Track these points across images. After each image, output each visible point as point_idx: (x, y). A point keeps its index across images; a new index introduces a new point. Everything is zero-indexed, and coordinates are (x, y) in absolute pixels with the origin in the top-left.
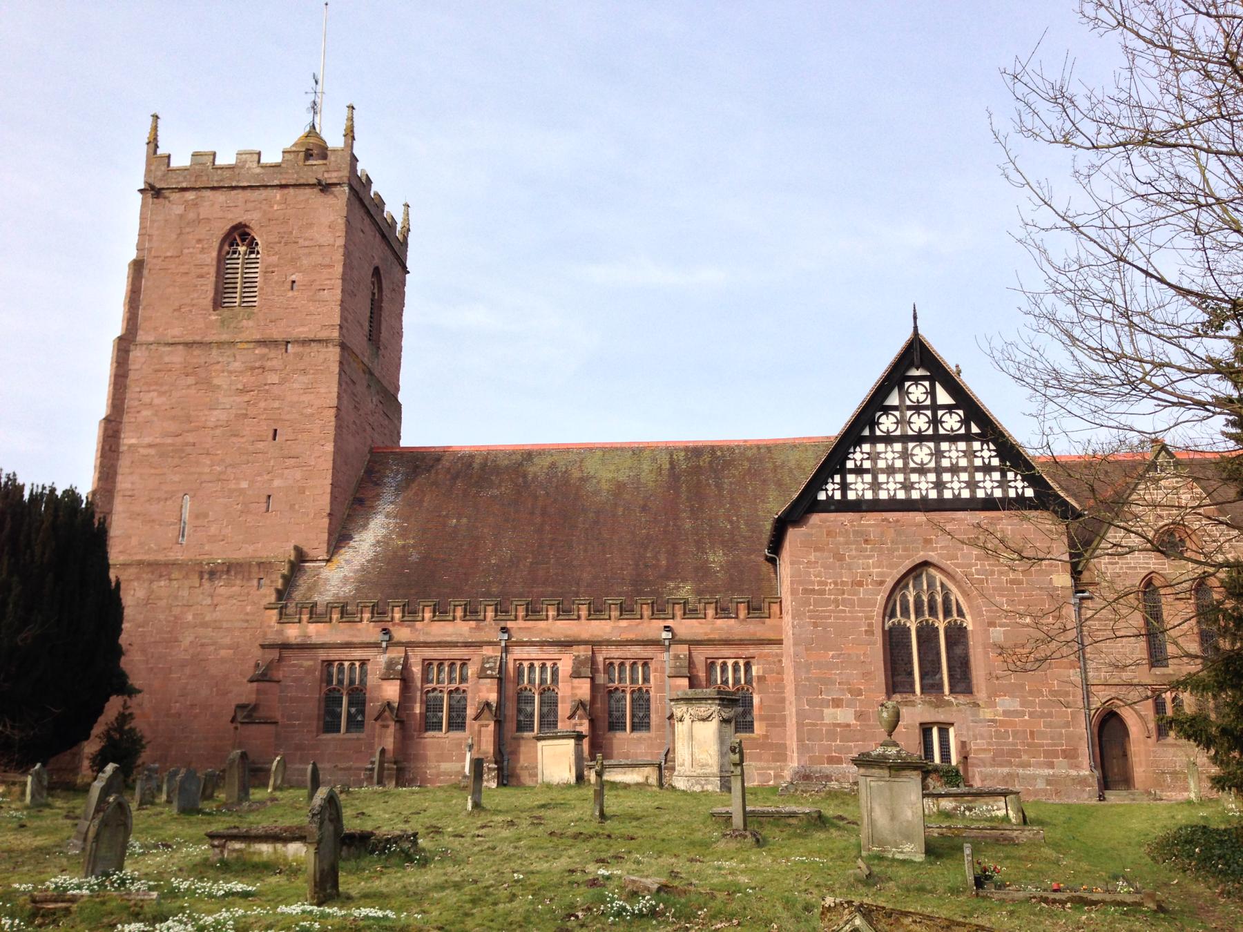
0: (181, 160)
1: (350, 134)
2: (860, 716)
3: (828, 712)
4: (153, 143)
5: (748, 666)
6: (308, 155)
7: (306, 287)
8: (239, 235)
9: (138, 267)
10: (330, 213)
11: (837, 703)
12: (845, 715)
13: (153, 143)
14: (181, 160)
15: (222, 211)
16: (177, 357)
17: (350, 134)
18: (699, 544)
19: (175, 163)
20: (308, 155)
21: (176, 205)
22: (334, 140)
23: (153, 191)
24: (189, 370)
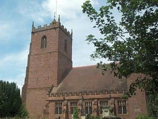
0: (37, 28)
1: (59, 20)
2: (142, 110)
3: (135, 110)
4: (33, 26)
5: (125, 102)
6: (53, 23)
7: (53, 44)
8: (45, 37)
9: (31, 44)
10: (55, 34)
11: (137, 108)
12: (139, 110)
13: (33, 26)
14: (37, 28)
15: (42, 34)
16: (36, 57)
17: (59, 20)
18: (152, 60)
19: (36, 28)
20: (53, 23)
21: (36, 35)
22: (57, 21)
23: (32, 33)
24: (38, 58)
